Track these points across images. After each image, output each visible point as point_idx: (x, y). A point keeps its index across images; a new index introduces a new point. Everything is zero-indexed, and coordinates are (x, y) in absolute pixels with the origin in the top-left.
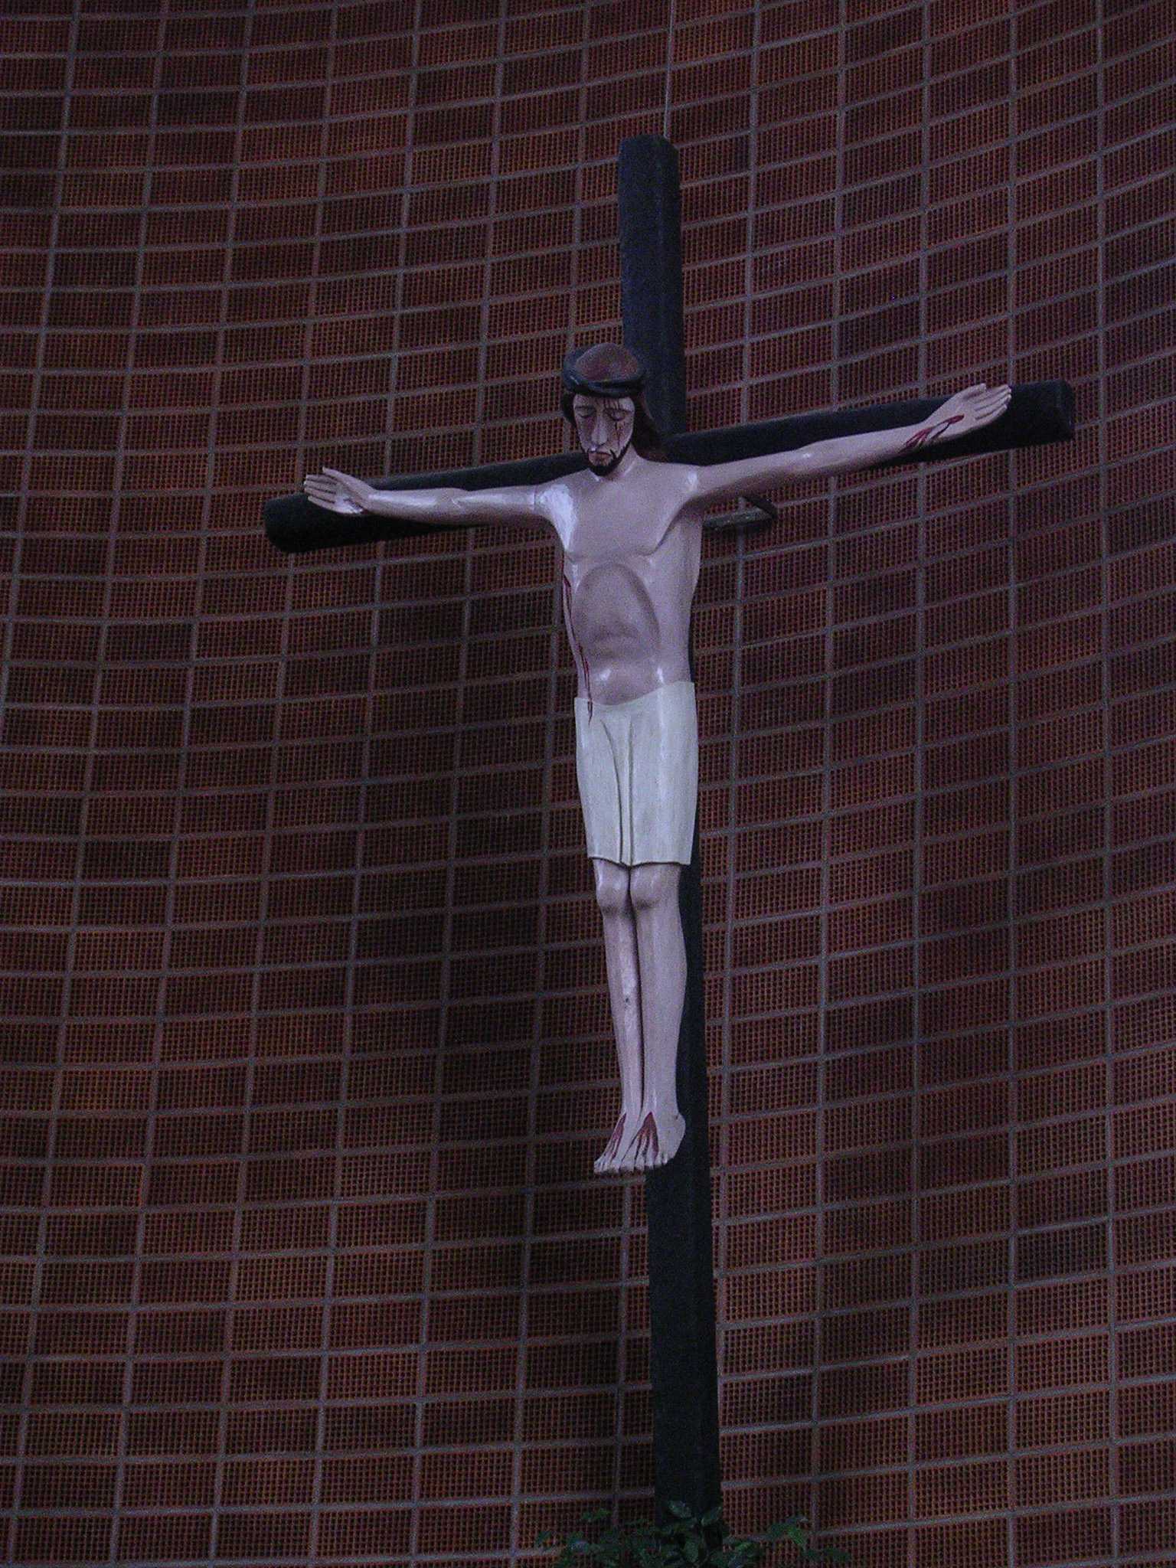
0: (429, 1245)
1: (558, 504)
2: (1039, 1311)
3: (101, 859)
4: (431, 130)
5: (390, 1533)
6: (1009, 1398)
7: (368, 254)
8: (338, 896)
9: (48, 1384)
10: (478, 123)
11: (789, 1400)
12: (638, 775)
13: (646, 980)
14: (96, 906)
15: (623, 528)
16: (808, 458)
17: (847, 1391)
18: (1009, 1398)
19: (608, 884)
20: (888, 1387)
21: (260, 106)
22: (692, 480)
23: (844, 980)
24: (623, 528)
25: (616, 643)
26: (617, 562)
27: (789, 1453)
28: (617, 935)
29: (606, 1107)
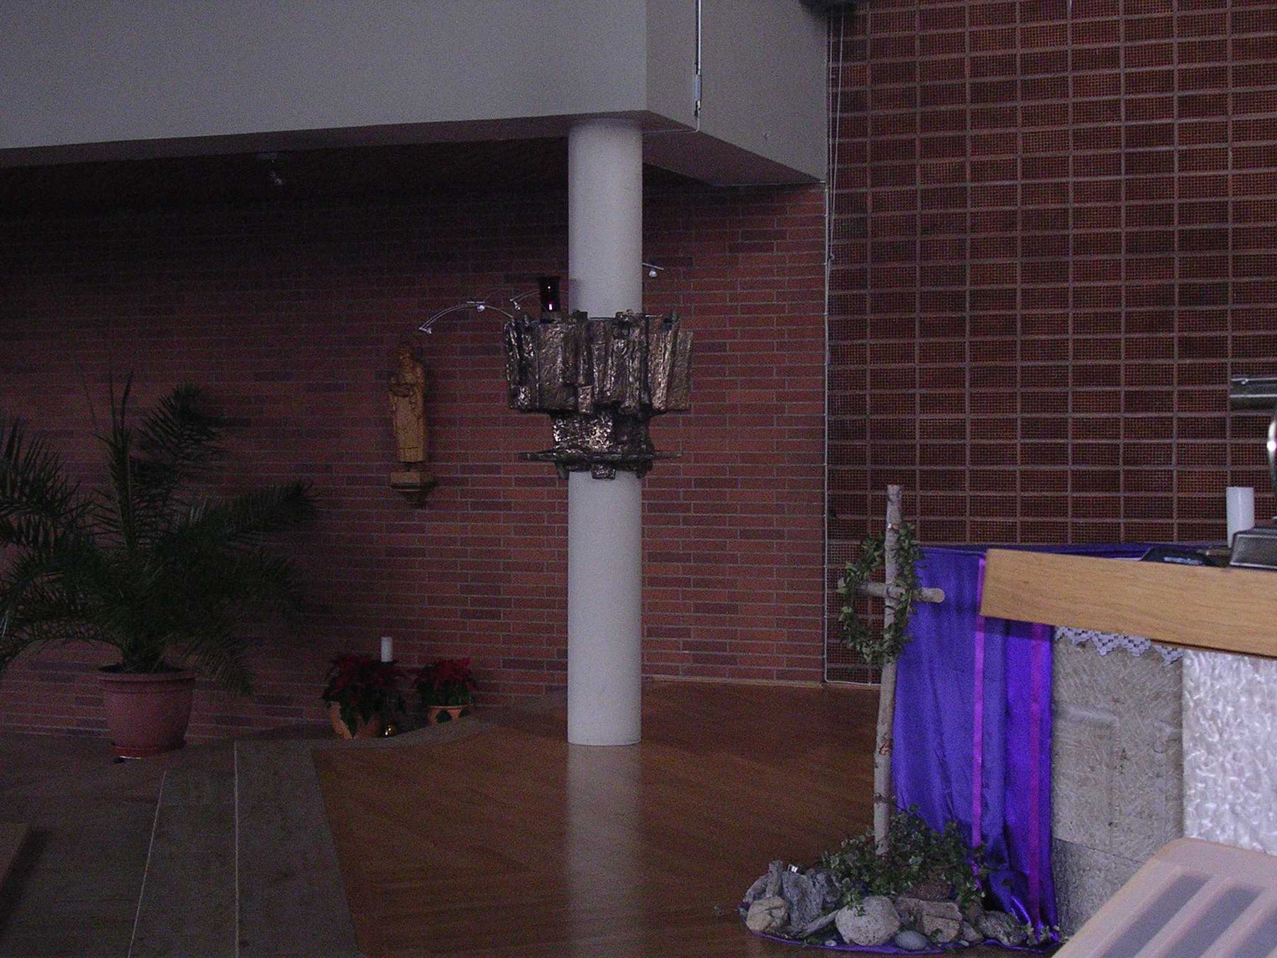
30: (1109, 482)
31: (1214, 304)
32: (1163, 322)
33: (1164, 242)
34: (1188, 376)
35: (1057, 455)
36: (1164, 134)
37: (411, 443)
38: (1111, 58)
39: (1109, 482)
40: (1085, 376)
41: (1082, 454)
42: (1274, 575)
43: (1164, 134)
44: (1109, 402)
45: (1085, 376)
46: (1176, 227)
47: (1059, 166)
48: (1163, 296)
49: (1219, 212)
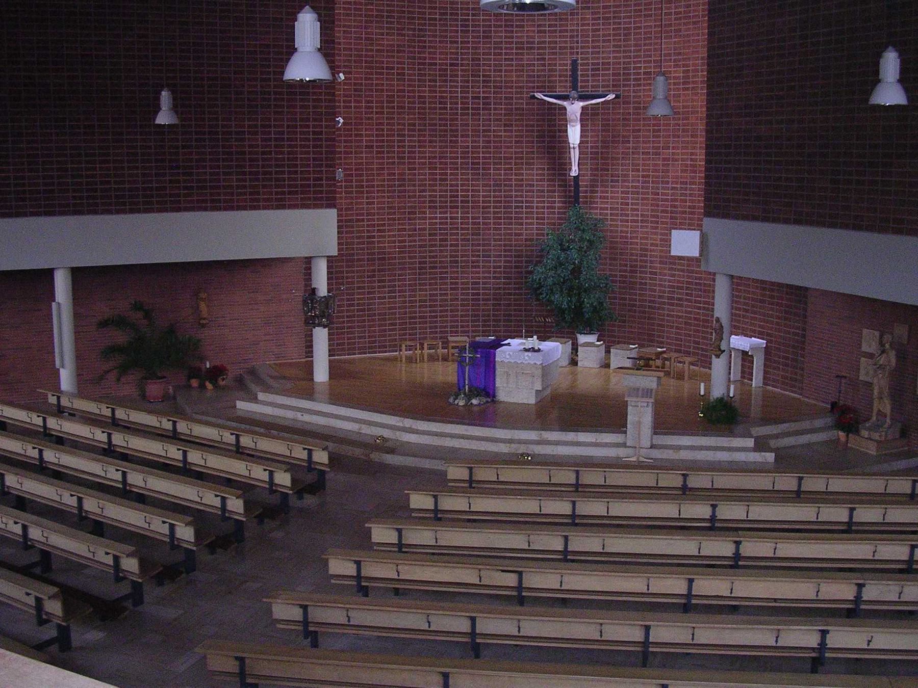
0: (546, 172)
1: (565, 103)
2: (612, 187)
3: (505, 125)
4: (539, 32)
5: (452, 3)
6: (609, 195)
7: (531, 48)
8: (533, 131)
9: (505, 185)
10: (545, 32)
11: (586, 192)
12: (574, 134)
13: (575, 156)
14: (505, 131)
15: (574, 108)
16: (594, 102)
17: (592, 192)
18: (609, 195)
19: (571, 146)
20: (597, 192)
21: (517, 26)
22: (582, 104)
23: (592, 147)
24: (574, 108)
25: (571, 121)
26: (574, 113)
27: (586, 197)
28: (572, 150)
29: (570, 169)
30: (364, 310)
31: (588, 649)
32: (374, 276)
33: (374, 260)
34: (379, 287)
35: (353, 305)
36: (374, 237)
37: (732, 387)
38: (363, 220)
39: (364, 310)
40: (359, 288)
41: (358, 305)
42: (915, 238)
43: (374, 237)
44: (364, 293)
45: (359, 288)
46: (311, 129)
47: (353, 243)
48: (374, 271)
49: (384, 253)
